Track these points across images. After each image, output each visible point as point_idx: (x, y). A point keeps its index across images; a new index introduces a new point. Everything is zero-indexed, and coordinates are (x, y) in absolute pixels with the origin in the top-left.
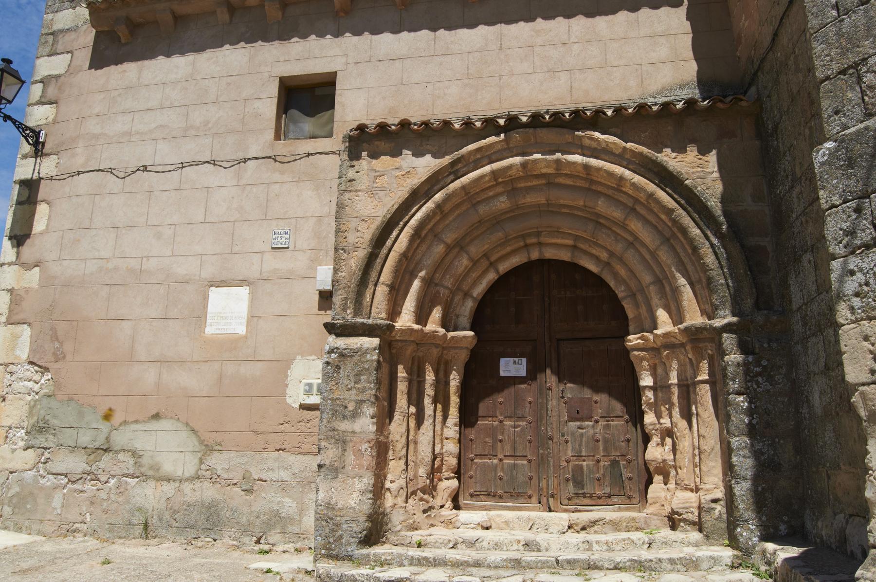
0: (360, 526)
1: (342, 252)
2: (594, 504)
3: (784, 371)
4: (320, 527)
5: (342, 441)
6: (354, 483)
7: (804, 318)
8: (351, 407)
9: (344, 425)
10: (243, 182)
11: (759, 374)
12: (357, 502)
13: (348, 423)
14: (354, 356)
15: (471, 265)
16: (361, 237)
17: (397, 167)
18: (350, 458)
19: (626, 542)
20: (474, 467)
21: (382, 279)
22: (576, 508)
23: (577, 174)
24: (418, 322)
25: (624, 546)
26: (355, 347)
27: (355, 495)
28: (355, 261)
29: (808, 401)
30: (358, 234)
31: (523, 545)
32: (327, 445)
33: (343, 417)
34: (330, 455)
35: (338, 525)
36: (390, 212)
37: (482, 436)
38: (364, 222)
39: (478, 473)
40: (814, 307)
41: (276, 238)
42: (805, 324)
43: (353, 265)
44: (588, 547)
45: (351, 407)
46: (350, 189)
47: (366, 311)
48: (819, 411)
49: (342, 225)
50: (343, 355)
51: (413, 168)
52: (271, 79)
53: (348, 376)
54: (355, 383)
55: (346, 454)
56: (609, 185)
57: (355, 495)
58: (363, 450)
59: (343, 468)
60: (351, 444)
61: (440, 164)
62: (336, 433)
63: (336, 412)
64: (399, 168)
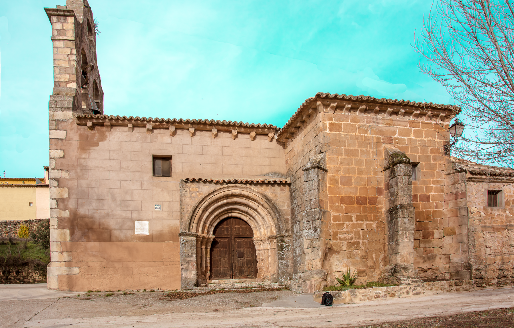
0: (194, 282)
3: (291, 246)
5: (188, 263)
7: (296, 235)
8: (190, 254)
9: (189, 259)
10: (143, 188)
11: (285, 247)
15: (68, 232)
21: (195, 222)
24: (202, 233)
27: (192, 275)
28: (187, 217)
29: (295, 252)
34: (185, 266)
35: (189, 282)
41: (156, 207)
42: (296, 237)
45: (190, 254)
47: (191, 230)
48: (297, 254)
50: (187, 241)
52: (150, 155)
57: (192, 275)
64: (198, 191)
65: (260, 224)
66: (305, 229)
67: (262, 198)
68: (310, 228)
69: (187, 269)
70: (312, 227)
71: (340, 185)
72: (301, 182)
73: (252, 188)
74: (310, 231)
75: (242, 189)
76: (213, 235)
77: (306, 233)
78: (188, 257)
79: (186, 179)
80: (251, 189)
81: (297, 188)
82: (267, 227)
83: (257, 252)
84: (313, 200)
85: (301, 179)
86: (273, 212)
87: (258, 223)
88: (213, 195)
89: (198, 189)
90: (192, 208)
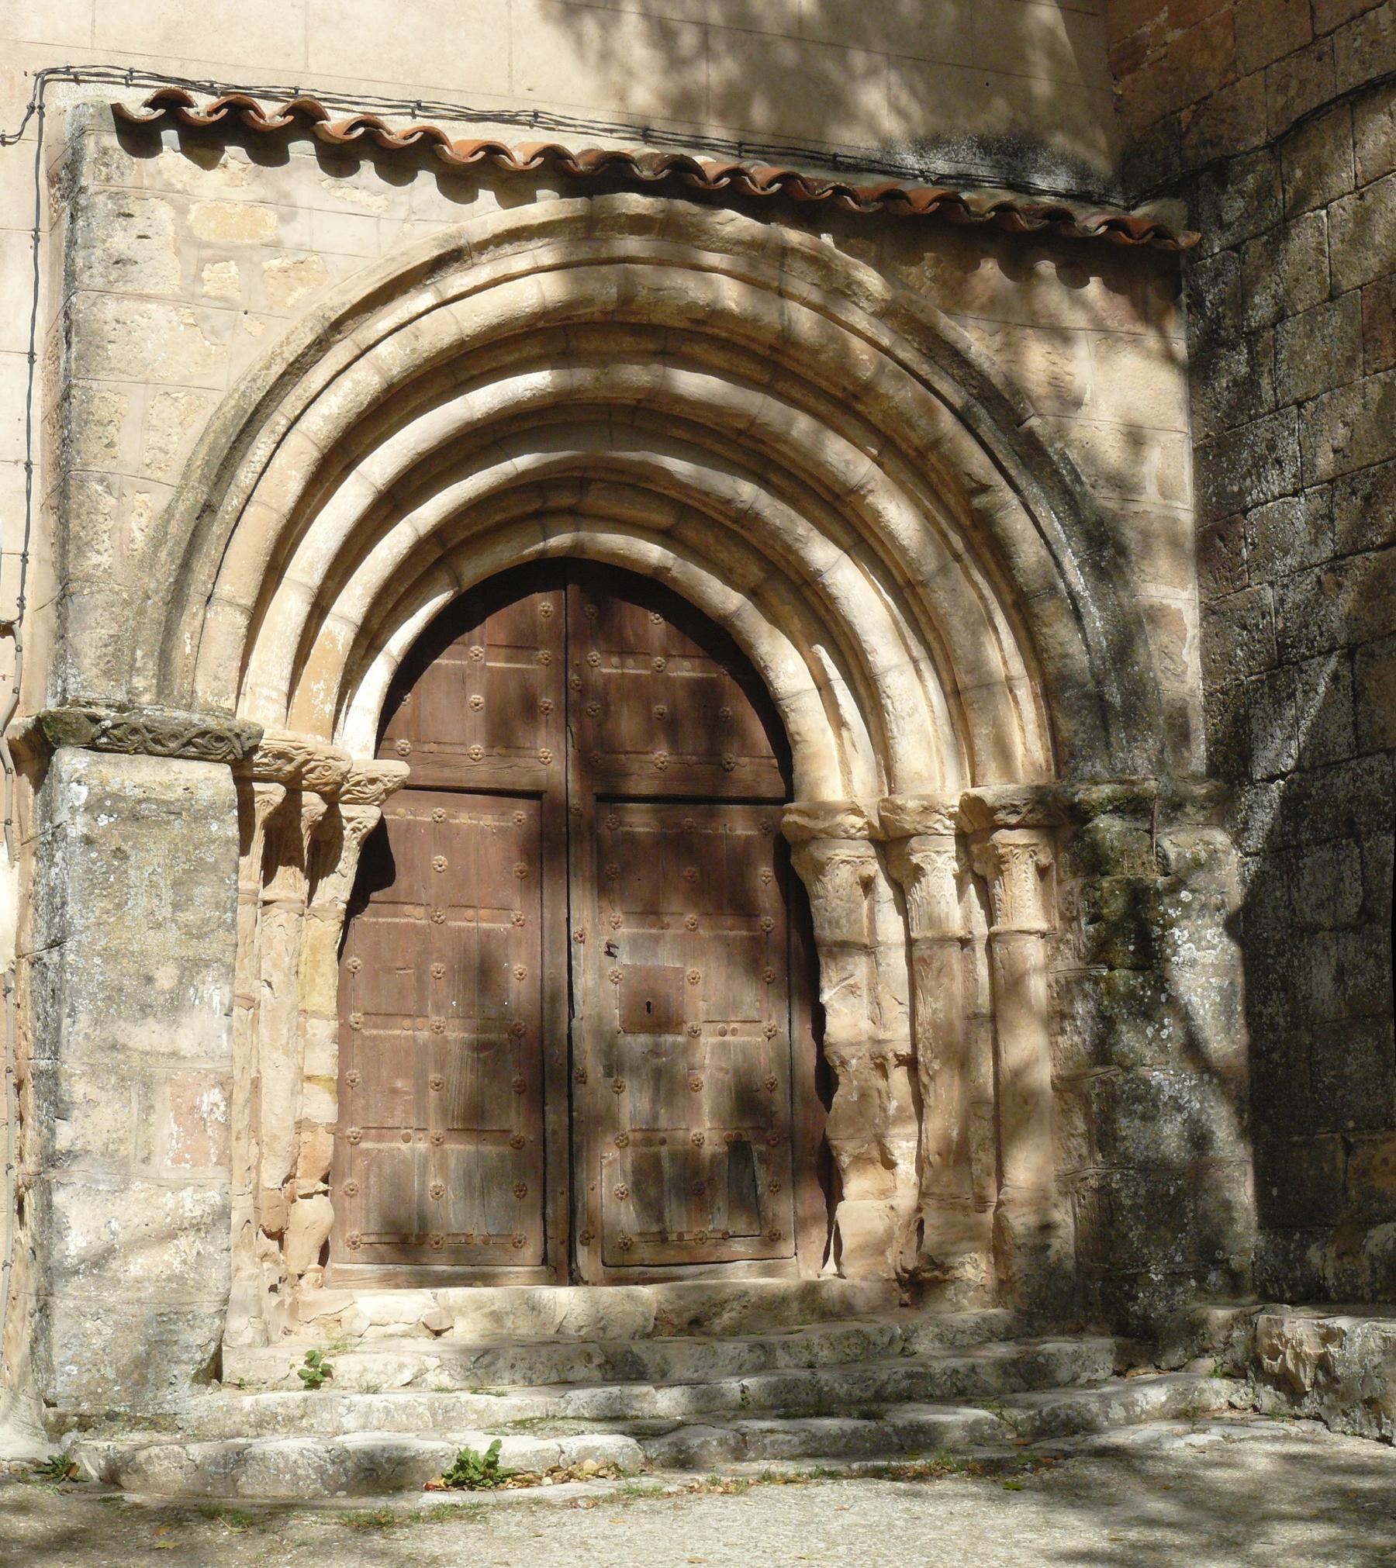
1: (99, 488)
2: (687, 1260)
4: (75, 1336)
8: (166, 978)
9: (146, 1035)
12: (191, 1259)
13: (157, 1028)
14: (168, 823)
16: (160, 449)
17: (266, 240)
18: (166, 1132)
19: (853, 1340)
20: (361, 1164)
22: (642, 1273)
23: (744, 342)
25: (848, 1351)
26: (170, 796)
30: (153, 438)
31: (599, 1366)
32: (94, 1093)
33: (142, 1010)
36: (259, 382)
37: (384, 1073)
38: (168, 402)
39: (373, 1180)
40: (1339, 782)
43: (138, 535)
44: (763, 1359)
45: (166, 978)
46: (120, 287)
47: (180, 684)
49: (96, 401)
51: (316, 253)
53: (153, 885)
54: (176, 906)
55: (153, 1118)
56: (820, 388)
58: (205, 1108)
59: (146, 1160)
60: (168, 1090)
61: (404, 258)
62: (121, 1057)
63: (121, 990)
64: (275, 245)
69: (124, 1163)
78: (145, 1009)
79: (153, 104)
89: (272, 217)
90: (198, 423)
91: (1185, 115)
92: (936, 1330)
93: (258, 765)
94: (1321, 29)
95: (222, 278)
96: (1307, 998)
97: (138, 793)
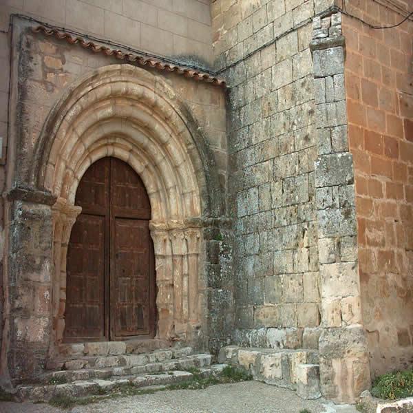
6: (40, 321)
8: (38, 262)
65: (170, 184)
66: (321, 207)
67: (180, 113)
68: (333, 207)
70: (337, 201)
71: (362, 103)
72: (262, 85)
73: (166, 86)
74: (332, 212)
75: (146, 84)
76: (76, 204)
77: (324, 218)
80: (163, 86)
81: (250, 99)
82: (183, 194)
83: (159, 262)
84: (337, 128)
85: (262, 79)
86: (198, 156)
87: (164, 182)
88: (90, 88)
91: (227, 52)
92: (41, 372)
93: (13, 207)
94: (255, 32)
95: (51, 76)
96: (247, 272)
97: (32, 212)
